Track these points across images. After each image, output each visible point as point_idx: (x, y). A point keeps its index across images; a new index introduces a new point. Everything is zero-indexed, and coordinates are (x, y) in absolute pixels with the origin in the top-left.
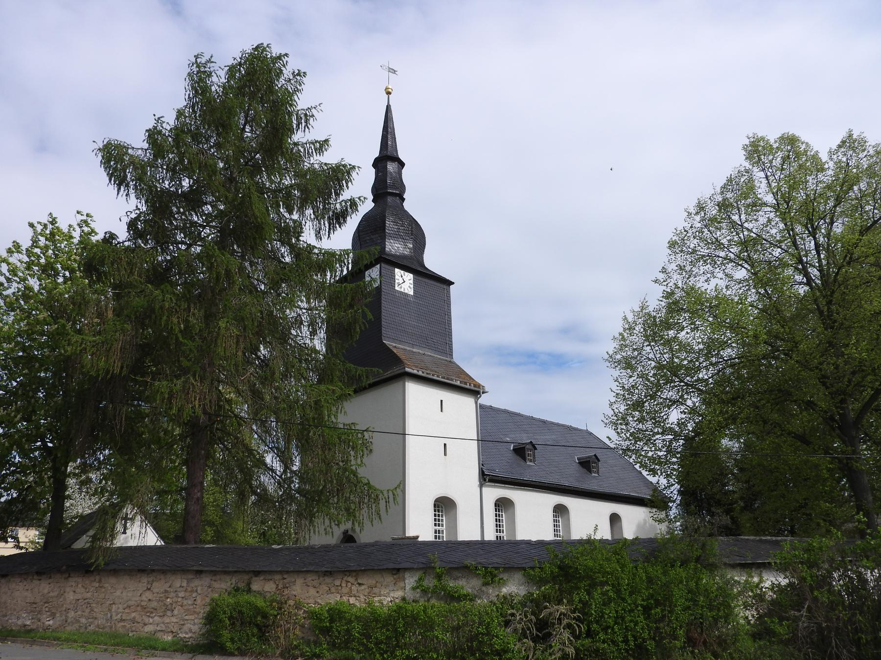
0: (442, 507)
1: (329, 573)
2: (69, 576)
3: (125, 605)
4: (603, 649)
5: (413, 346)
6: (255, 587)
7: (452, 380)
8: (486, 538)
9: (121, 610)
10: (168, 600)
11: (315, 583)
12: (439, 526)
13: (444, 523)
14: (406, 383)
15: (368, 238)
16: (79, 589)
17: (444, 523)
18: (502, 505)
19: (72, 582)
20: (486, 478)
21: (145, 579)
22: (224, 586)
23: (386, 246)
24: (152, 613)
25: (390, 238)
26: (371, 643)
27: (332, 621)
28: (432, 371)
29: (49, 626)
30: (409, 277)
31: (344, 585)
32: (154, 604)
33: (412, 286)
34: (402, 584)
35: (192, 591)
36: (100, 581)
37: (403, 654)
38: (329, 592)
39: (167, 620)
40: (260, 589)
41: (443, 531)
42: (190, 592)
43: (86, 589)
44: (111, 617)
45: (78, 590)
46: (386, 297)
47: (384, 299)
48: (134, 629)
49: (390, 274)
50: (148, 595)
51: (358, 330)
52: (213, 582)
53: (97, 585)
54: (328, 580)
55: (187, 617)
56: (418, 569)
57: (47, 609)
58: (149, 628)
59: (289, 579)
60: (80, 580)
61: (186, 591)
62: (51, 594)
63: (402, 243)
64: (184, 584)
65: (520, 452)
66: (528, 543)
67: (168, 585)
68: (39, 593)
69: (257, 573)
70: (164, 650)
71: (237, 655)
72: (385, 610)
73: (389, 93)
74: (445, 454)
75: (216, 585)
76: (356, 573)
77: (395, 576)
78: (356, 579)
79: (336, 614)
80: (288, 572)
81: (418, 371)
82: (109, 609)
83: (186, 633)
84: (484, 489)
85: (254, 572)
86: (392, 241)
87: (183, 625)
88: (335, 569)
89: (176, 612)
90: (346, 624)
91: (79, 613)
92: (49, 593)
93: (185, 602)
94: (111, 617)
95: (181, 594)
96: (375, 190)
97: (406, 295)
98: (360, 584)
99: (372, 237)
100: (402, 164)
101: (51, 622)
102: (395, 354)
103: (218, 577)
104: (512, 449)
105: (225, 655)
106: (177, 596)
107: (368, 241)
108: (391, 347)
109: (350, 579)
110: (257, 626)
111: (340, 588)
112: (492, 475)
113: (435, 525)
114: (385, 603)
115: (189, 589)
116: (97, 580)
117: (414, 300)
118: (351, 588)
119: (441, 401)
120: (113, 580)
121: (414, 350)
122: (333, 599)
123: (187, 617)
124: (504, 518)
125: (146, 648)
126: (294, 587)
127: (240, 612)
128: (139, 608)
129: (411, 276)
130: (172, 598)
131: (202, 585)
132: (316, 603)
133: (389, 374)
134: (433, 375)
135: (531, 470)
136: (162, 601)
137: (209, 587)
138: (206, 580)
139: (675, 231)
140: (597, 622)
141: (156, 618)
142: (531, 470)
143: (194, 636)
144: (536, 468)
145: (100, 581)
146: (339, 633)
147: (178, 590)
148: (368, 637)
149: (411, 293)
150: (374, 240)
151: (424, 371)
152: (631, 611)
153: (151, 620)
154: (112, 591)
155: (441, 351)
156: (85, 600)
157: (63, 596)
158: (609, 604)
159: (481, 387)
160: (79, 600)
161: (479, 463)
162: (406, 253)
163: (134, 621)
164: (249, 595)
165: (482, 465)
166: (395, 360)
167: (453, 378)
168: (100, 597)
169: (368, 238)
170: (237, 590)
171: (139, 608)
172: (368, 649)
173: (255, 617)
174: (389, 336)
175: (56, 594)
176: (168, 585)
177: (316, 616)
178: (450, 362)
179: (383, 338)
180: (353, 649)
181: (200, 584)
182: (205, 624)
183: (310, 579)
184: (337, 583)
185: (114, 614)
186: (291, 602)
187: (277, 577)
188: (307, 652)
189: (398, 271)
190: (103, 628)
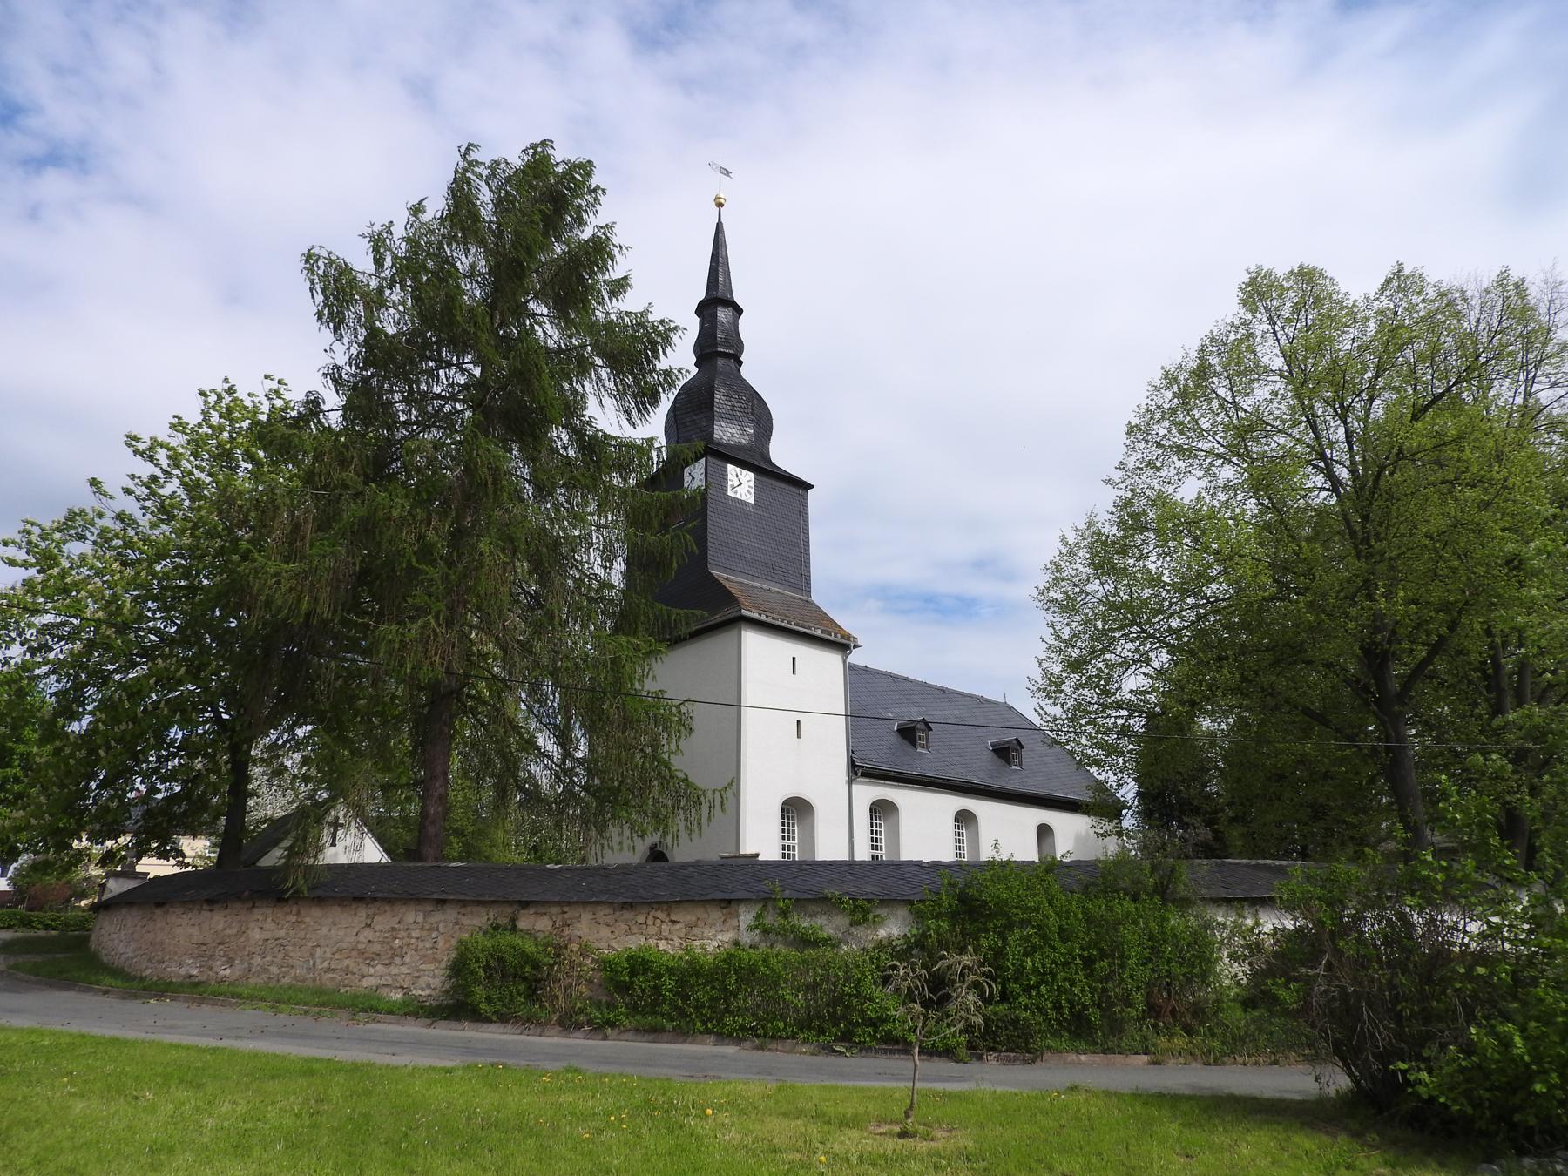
0: (793, 813)
1: (628, 906)
3: (335, 949)
6: (522, 924)
7: (810, 628)
8: (858, 857)
9: (328, 955)
10: (397, 941)
11: (610, 919)
12: (788, 839)
13: (796, 835)
15: (688, 419)
16: (269, 925)
17: (796, 835)
18: (881, 810)
19: (258, 914)
20: (859, 770)
22: (477, 922)
24: (373, 959)
27: (633, 974)
30: (748, 477)
31: (650, 922)
32: (376, 947)
33: (752, 491)
34: (734, 922)
35: (431, 930)
36: (298, 914)
37: (734, 1022)
38: (629, 932)
39: (394, 970)
41: (794, 847)
44: (314, 965)
48: (347, 982)
53: (294, 919)
54: (627, 915)
55: (423, 967)
56: (757, 901)
57: (222, 953)
59: (571, 913)
60: (269, 911)
61: (422, 929)
62: (228, 932)
64: (420, 919)
65: (908, 733)
66: (918, 865)
67: (397, 919)
69: (525, 904)
70: (390, 1013)
72: (711, 959)
73: (720, 205)
74: (799, 736)
75: (466, 921)
77: (724, 911)
79: (640, 964)
80: (569, 903)
81: (760, 614)
83: (423, 989)
85: (520, 902)
86: (723, 424)
87: (419, 977)
89: (407, 959)
91: (268, 958)
92: (225, 929)
93: (421, 945)
94: (314, 965)
95: (415, 934)
97: (743, 503)
98: (673, 922)
99: (695, 417)
101: (228, 972)
105: (477, 1021)
106: (409, 937)
109: (660, 914)
111: (644, 926)
113: (783, 838)
114: (710, 949)
115: (427, 927)
116: (294, 912)
118: (660, 928)
119: (794, 658)
120: (316, 912)
121: (755, 584)
122: (635, 942)
123: (423, 967)
126: (578, 925)
127: (500, 960)
128: (355, 953)
129: (750, 475)
131: (445, 921)
133: (717, 618)
134: (782, 621)
135: (924, 761)
137: (456, 923)
138: (451, 914)
139: (1137, 410)
145: (298, 914)
146: (643, 991)
156: (276, 940)
157: (245, 935)
161: (848, 750)
163: (347, 971)
166: (728, 598)
167: (811, 625)
170: (496, 927)
171: (355, 953)
173: (523, 967)
175: (235, 931)
176: (397, 919)
180: (662, 1015)
181: (444, 919)
182: (450, 977)
184: (641, 919)
185: (318, 961)
186: (575, 947)
187: (554, 910)
189: (730, 467)
190: (303, 981)
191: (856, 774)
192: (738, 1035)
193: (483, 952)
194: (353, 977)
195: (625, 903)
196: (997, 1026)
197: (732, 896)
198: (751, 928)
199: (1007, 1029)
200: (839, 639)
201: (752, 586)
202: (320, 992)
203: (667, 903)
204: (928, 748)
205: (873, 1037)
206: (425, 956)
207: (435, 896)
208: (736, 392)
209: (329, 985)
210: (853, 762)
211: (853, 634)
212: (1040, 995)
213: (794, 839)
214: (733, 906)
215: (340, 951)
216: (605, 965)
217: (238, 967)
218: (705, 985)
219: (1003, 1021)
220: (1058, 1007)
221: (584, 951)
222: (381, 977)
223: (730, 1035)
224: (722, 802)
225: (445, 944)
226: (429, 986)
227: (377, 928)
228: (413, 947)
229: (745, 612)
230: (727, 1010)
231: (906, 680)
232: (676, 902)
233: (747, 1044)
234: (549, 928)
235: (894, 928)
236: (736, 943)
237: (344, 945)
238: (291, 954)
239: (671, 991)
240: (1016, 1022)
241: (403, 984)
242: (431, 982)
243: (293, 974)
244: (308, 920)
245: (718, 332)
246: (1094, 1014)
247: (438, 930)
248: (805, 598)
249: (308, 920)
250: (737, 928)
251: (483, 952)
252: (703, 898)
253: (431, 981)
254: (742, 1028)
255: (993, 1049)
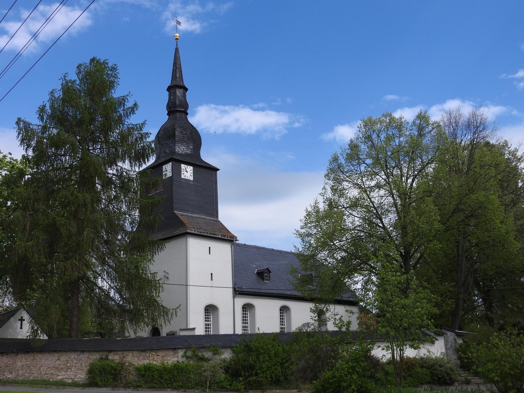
0: (210, 310)
1: (144, 351)
2: (17, 354)
3: (47, 367)
4: (261, 380)
5: (193, 213)
6: (110, 357)
7: (216, 235)
9: (45, 369)
10: (69, 364)
11: (138, 355)
12: (208, 321)
13: (211, 320)
14: (188, 239)
15: (164, 142)
16: (24, 360)
17: (211, 320)
18: (247, 308)
19: (19, 356)
20: (238, 292)
21: (56, 355)
22: (95, 357)
23: (176, 148)
24: (61, 370)
25: (178, 143)
26: (163, 380)
27: (145, 371)
28: (204, 230)
29: (10, 377)
30: (190, 169)
31: (151, 356)
32: (62, 366)
33: (192, 175)
34: (177, 355)
35: (80, 360)
36: (34, 356)
37: (176, 384)
38: (144, 359)
39: (68, 373)
40: (112, 358)
41: (210, 324)
42: (79, 360)
43: (27, 360)
44: (41, 373)
45: (23, 361)
46: (176, 183)
47: (175, 185)
48: (52, 378)
49: (178, 168)
50: (59, 362)
51: (156, 226)
52: (90, 356)
53: (32, 358)
54: (143, 354)
55: (78, 372)
56: (184, 348)
57: (7, 370)
58: (60, 377)
59: (125, 353)
60: (23, 356)
61: (77, 360)
62: (9, 363)
63: (186, 146)
64: (76, 357)
65: (261, 275)
67: (68, 357)
68: (2, 362)
69: (110, 351)
70: (69, 386)
71: (103, 387)
72: (169, 366)
74: (212, 280)
75: (91, 357)
76: (157, 350)
77: (174, 352)
78: (156, 353)
79: (148, 369)
80: (125, 351)
81: (195, 231)
82: (39, 369)
83: (78, 379)
84: (235, 299)
85: (109, 351)
86: (179, 145)
87: (77, 375)
88: (147, 349)
89: (72, 370)
90: (152, 373)
91: (24, 371)
92: (8, 362)
93: (77, 365)
94: (41, 373)
95: (75, 361)
96: (168, 108)
97: (189, 180)
98: (158, 355)
99: (167, 142)
100: (186, 89)
101: (10, 376)
102: (181, 220)
103: (92, 353)
104: (256, 272)
105: (98, 387)
106: (73, 362)
107: (164, 144)
108: (179, 215)
109: (154, 353)
110: (112, 374)
111: (149, 357)
112: (240, 291)
113: (206, 321)
114: (169, 363)
115: (79, 359)
116: (32, 356)
117: (194, 184)
118: (154, 357)
119: (210, 248)
120: (40, 355)
121: (194, 215)
122: (146, 362)
123: (78, 372)
124: (248, 316)
125: (61, 385)
126: (128, 357)
127: (104, 369)
128: (54, 368)
129: (192, 168)
130: (70, 363)
131: (84, 357)
132: (138, 364)
133: (177, 232)
134: (204, 233)
135: (267, 286)
136: (65, 365)
137: (88, 358)
138: (86, 355)
139: (327, 168)
140: (260, 370)
141: (63, 373)
142: (267, 286)
143: (82, 380)
144: (270, 284)
145: (34, 356)
146: (149, 376)
147: (73, 359)
148: (162, 378)
149: (192, 179)
150: (168, 143)
151: (198, 230)
152: (274, 365)
153: (61, 374)
154: (40, 360)
155: (211, 214)
156: (27, 365)
157: (15, 364)
158: (333, 363)
159: (235, 238)
160: (23, 365)
161: (233, 282)
162: (188, 152)
163: (52, 374)
164: (107, 361)
165: (235, 285)
166: (182, 224)
167: (217, 233)
168: (35, 363)
169: (164, 142)
170: (101, 359)
171: (54, 368)
172: (161, 383)
173: (111, 371)
174: (177, 208)
175: (11, 362)
176: (68, 357)
177: (139, 369)
178: (216, 221)
179: (174, 209)
180: (155, 383)
181: (84, 357)
182: (88, 374)
183: (135, 353)
184: (148, 355)
185: (42, 371)
186: (127, 364)
187: (120, 353)
188: (135, 385)
189: (182, 165)
190: (37, 378)
191: (236, 294)
192: (177, 388)
193: (98, 366)
194: (54, 376)
195: (142, 350)
196: (253, 383)
197: (177, 347)
198: (182, 357)
199: (256, 383)
200: (229, 239)
201: (192, 217)
202: (45, 381)
203: (156, 350)
204: (269, 280)
205: (217, 387)
206: (78, 368)
207: (81, 350)
208: (185, 130)
209: (47, 379)
210: (235, 289)
211: (236, 235)
212: (267, 374)
213: (248, 324)
214: (176, 351)
215: (49, 368)
216: (138, 369)
217: (14, 374)
218: (167, 374)
219: (255, 381)
220: (271, 377)
221: (131, 364)
222: (64, 375)
223: (175, 388)
224: (176, 313)
225: (85, 364)
226: (80, 378)
227: (61, 360)
228: (74, 366)
229: (189, 231)
230: (174, 381)
231: (264, 248)
232: (158, 349)
233: (180, 391)
234: (119, 359)
235: (227, 355)
236: (178, 361)
237: (51, 366)
238: (32, 370)
239: (157, 376)
240: (258, 381)
241: (72, 377)
242: (81, 376)
243: (33, 376)
244: (37, 358)
245: (177, 101)
246: (282, 378)
247: (82, 360)
248: (215, 219)
249: (37, 358)
250: (178, 357)
251: (98, 366)
252: (168, 348)
253: (81, 376)
254: (179, 386)
255: (252, 389)
